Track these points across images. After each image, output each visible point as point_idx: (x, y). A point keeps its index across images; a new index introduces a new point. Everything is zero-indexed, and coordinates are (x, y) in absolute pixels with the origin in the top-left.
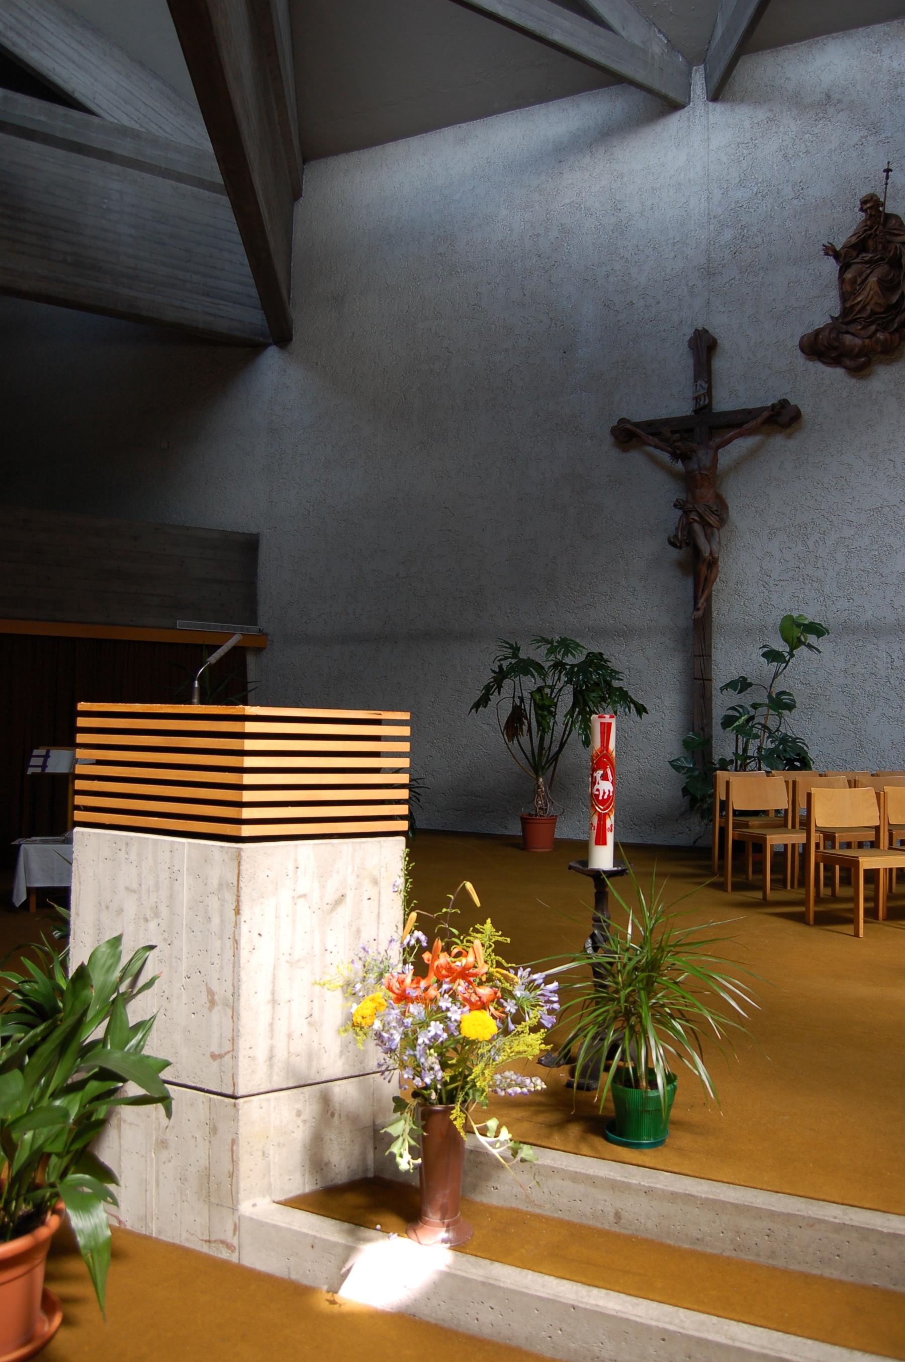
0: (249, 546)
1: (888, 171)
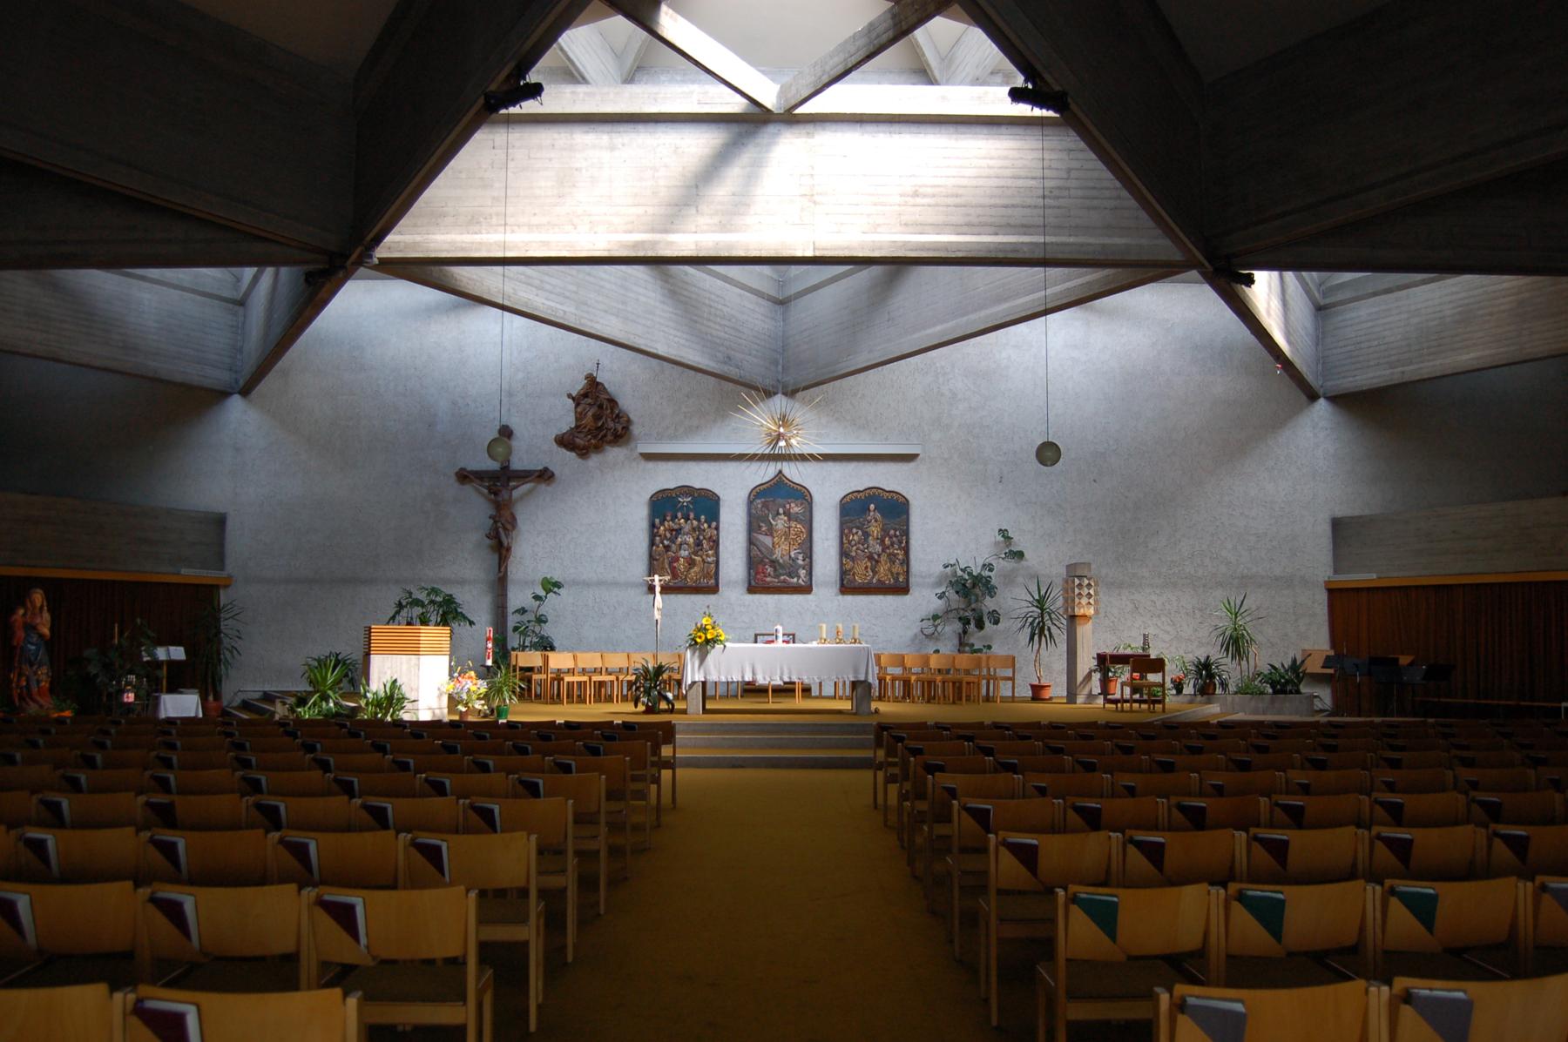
0: (220, 521)
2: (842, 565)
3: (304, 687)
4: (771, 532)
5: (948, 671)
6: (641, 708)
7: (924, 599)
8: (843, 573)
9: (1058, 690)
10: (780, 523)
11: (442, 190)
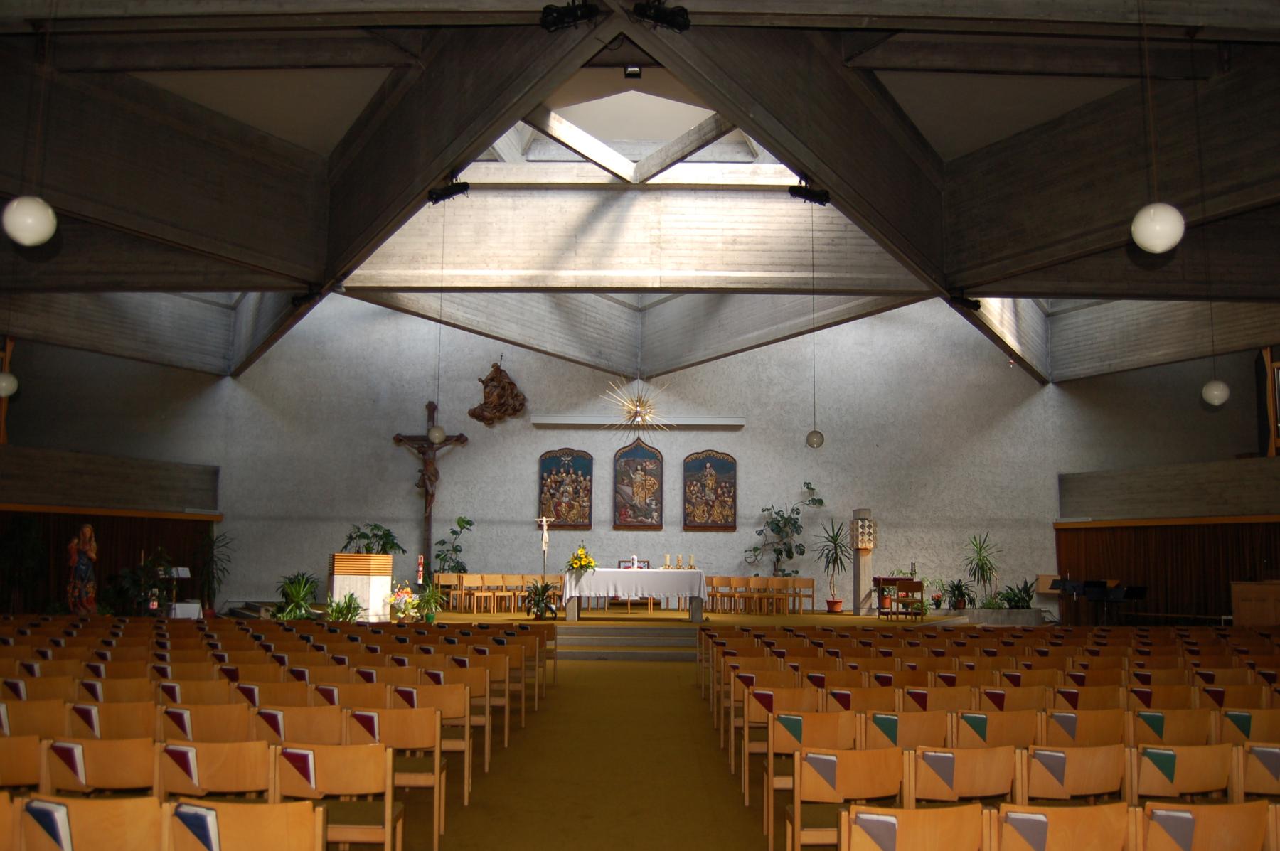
0: (214, 473)
2: (685, 508)
3: (279, 599)
4: (631, 484)
5: (765, 590)
6: (532, 616)
7: (747, 536)
8: (686, 515)
9: (847, 605)
10: (638, 477)
11: (398, 242)
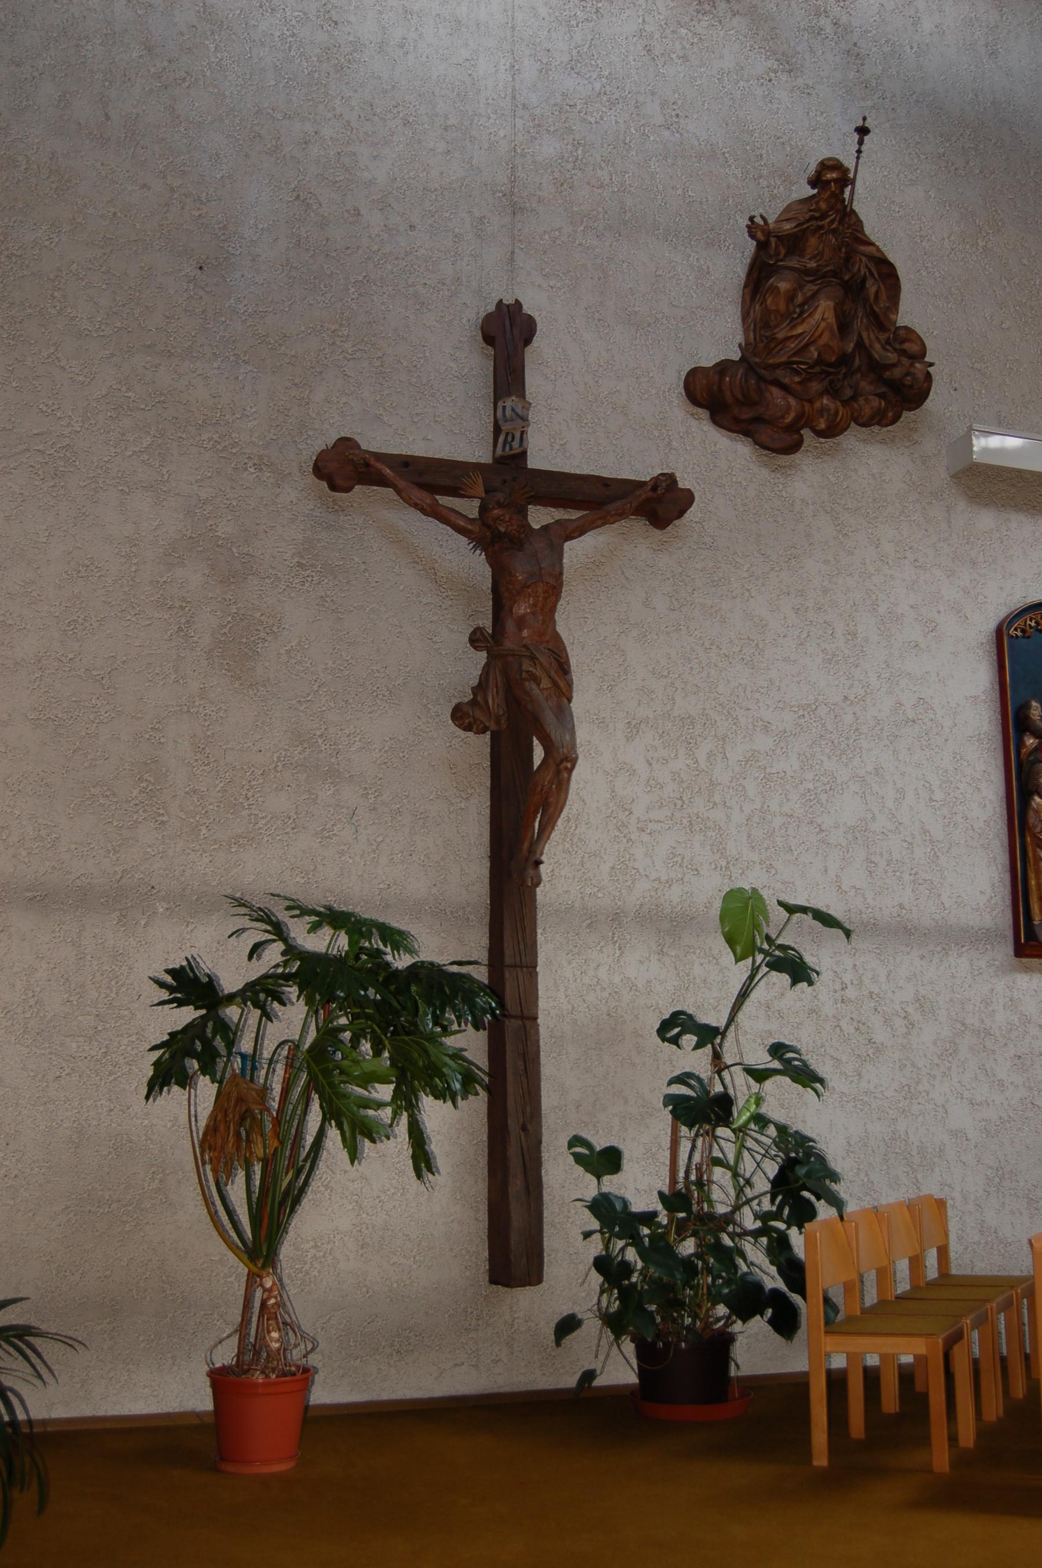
1: (863, 131)
